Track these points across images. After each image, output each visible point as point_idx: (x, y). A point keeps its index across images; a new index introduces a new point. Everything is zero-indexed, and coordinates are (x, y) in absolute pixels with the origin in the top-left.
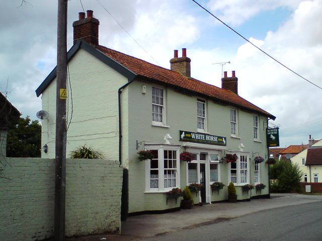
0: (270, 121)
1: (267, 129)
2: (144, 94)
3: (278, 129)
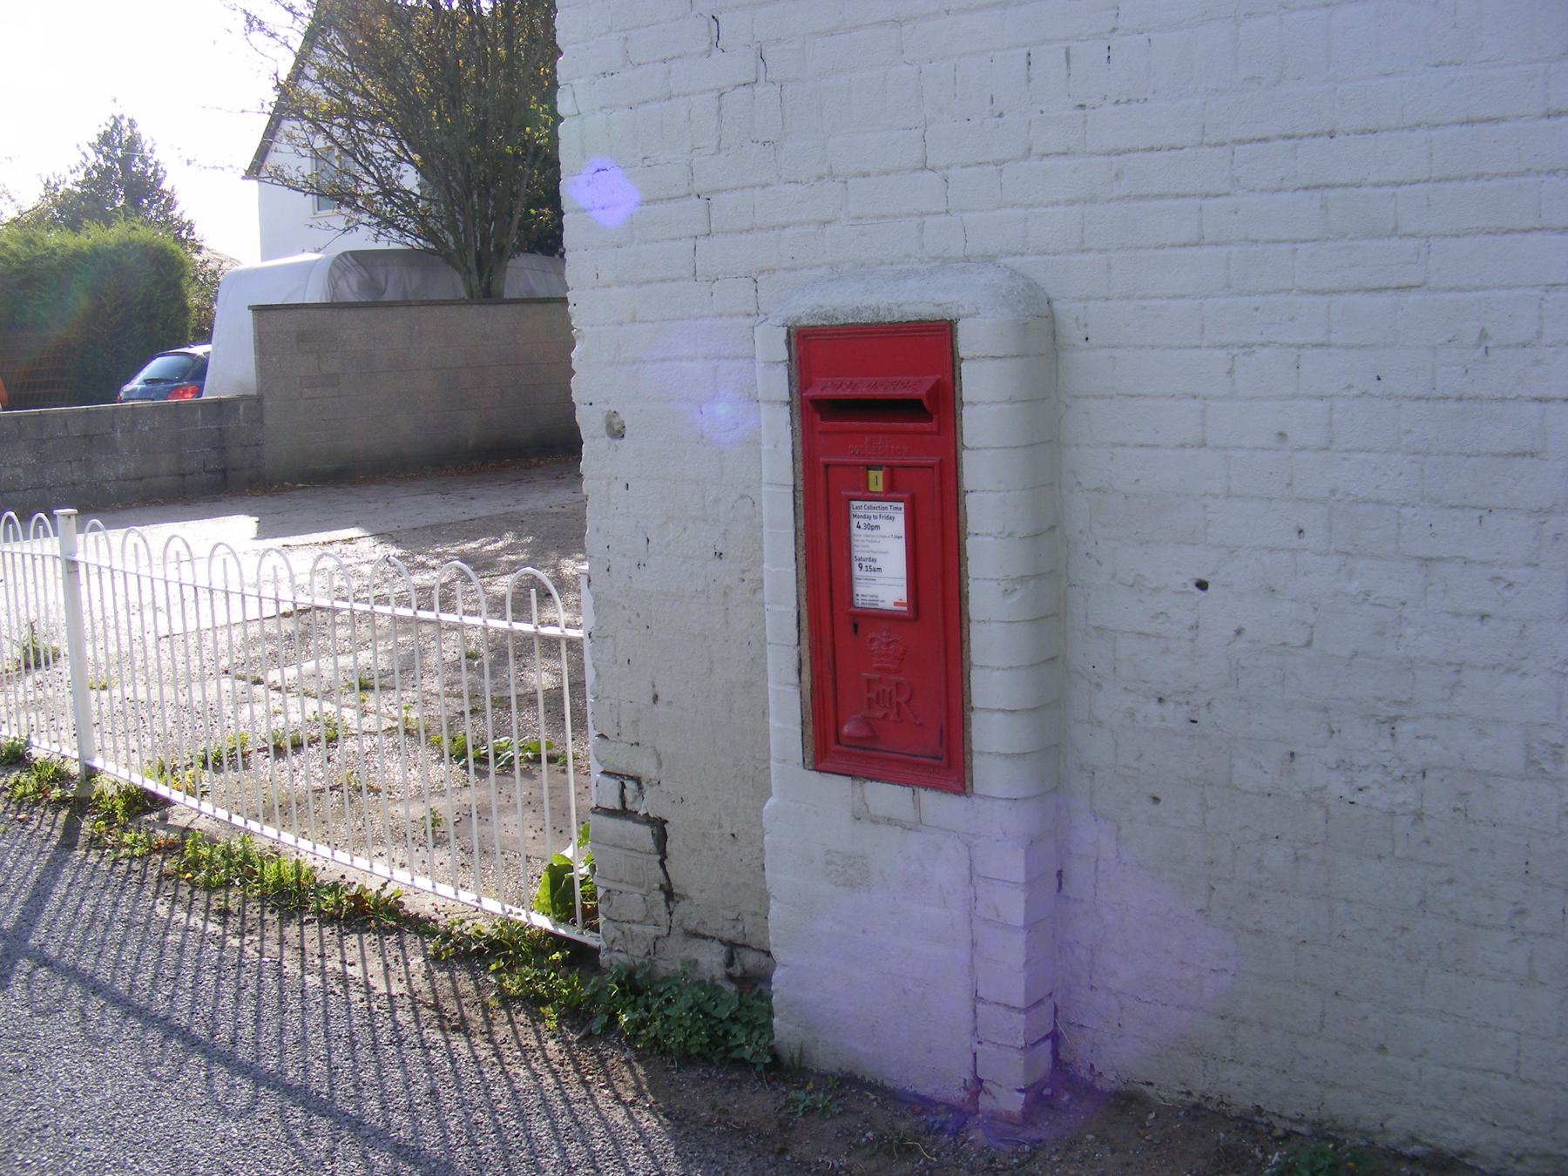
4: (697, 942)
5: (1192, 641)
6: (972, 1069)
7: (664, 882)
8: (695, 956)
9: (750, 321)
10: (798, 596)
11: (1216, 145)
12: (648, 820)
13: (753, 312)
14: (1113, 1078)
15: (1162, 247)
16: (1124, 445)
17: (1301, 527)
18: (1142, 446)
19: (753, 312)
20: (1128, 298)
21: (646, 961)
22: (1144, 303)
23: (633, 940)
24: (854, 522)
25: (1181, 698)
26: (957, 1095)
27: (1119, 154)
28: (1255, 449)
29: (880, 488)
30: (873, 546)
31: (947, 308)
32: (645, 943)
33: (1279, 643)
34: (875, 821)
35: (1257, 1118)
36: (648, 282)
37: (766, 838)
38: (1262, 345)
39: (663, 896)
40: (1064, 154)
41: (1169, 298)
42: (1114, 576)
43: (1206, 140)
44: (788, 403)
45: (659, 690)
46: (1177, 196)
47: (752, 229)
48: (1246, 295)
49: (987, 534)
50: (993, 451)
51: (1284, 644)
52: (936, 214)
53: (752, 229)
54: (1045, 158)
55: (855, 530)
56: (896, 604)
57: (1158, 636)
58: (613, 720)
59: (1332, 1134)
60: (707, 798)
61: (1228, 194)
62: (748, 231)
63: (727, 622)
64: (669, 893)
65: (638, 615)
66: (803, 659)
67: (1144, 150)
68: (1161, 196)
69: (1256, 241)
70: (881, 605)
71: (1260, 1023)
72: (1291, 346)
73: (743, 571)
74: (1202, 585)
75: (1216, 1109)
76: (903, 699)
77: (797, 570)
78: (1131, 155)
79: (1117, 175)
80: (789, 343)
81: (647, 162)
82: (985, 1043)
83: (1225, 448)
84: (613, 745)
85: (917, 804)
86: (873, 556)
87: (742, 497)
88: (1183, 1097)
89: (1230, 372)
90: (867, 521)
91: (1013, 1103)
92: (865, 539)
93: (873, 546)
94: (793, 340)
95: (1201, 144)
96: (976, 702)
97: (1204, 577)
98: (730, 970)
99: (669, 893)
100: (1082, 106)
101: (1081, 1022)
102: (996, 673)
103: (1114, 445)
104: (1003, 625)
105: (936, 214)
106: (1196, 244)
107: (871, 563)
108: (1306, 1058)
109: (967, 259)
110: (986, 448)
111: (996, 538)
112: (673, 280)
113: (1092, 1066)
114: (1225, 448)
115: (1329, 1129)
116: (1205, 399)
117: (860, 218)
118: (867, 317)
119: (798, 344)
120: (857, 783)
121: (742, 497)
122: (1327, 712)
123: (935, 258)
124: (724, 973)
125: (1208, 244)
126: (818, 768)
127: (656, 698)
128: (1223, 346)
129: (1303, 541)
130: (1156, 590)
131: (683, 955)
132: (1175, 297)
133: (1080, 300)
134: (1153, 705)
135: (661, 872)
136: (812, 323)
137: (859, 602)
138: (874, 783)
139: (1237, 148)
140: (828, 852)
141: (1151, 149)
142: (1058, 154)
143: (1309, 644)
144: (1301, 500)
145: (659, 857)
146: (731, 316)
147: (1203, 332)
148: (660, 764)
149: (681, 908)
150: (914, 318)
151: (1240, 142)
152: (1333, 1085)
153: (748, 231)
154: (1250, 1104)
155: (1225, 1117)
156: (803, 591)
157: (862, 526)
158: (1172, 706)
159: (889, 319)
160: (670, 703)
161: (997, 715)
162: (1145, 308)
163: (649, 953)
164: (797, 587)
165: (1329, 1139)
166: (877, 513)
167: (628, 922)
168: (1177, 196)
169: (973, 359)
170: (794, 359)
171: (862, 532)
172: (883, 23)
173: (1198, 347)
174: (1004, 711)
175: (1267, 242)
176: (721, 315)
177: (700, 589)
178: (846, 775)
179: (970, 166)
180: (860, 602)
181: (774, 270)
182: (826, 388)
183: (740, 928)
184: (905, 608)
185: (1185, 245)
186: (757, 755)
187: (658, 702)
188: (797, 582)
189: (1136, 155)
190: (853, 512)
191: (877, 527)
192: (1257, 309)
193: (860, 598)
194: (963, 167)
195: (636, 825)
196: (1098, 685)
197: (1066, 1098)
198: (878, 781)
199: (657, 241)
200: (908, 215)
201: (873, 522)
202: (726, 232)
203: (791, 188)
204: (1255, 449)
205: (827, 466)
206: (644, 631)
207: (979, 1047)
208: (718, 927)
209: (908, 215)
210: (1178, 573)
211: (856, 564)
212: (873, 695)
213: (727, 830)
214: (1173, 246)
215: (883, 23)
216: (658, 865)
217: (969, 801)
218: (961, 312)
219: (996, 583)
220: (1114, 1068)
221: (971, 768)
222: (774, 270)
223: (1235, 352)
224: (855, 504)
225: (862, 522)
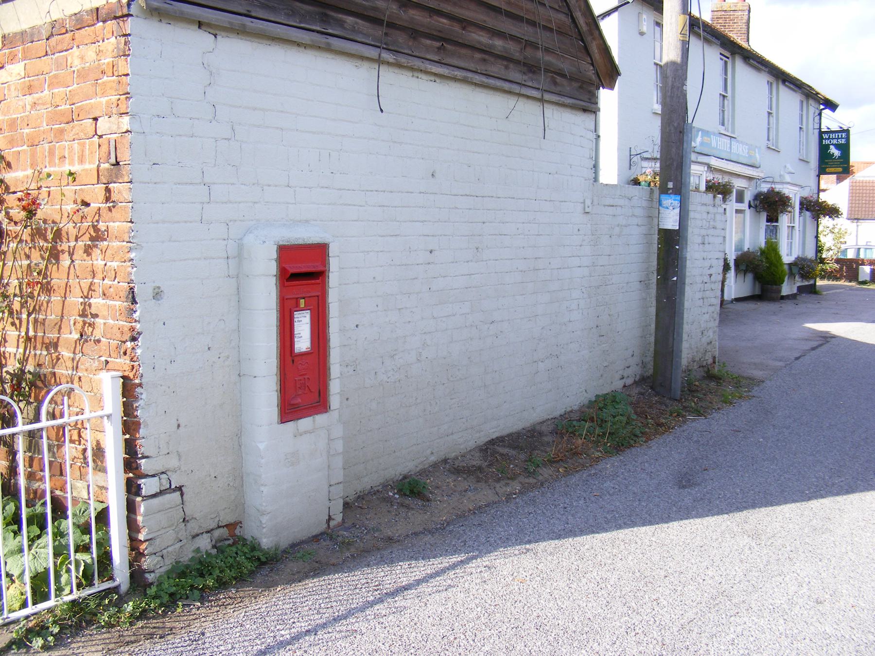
0: (827, 112)
1: (821, 133)
2: (642, 34)
3: (847, 132)
8: (198, 546)
9: (225, 242)
13: (226, 238)
19: (226, 238)
36: (178, 222)
44: (275, 275)
45: (180, 422)
56: (306, 349)
58: (156, 446)
62: (226, 203)
70: (302, 350)
73: (220, 354)
81: (181, 165)
84: (155, 459)
86: (300, 332)
87: (220, 320)
100: (332, 173)
118: (301, 242)
121: (220, 320)
123: (292, 220)
127: (179, 426)
139: (367, 193)
151: (367, 191)
153: (226, 203)
172: (277, 128)
176: (213, 239)
181: (236, 221)
182: (293, 269)
187: (180, 428)
190: (295, 316)
201: (300, 319)
203: (243, 186)
206: (173, 394)
215: (277, 128)
221: (329, 402)
222: (236, 221)
224: (295, 313)
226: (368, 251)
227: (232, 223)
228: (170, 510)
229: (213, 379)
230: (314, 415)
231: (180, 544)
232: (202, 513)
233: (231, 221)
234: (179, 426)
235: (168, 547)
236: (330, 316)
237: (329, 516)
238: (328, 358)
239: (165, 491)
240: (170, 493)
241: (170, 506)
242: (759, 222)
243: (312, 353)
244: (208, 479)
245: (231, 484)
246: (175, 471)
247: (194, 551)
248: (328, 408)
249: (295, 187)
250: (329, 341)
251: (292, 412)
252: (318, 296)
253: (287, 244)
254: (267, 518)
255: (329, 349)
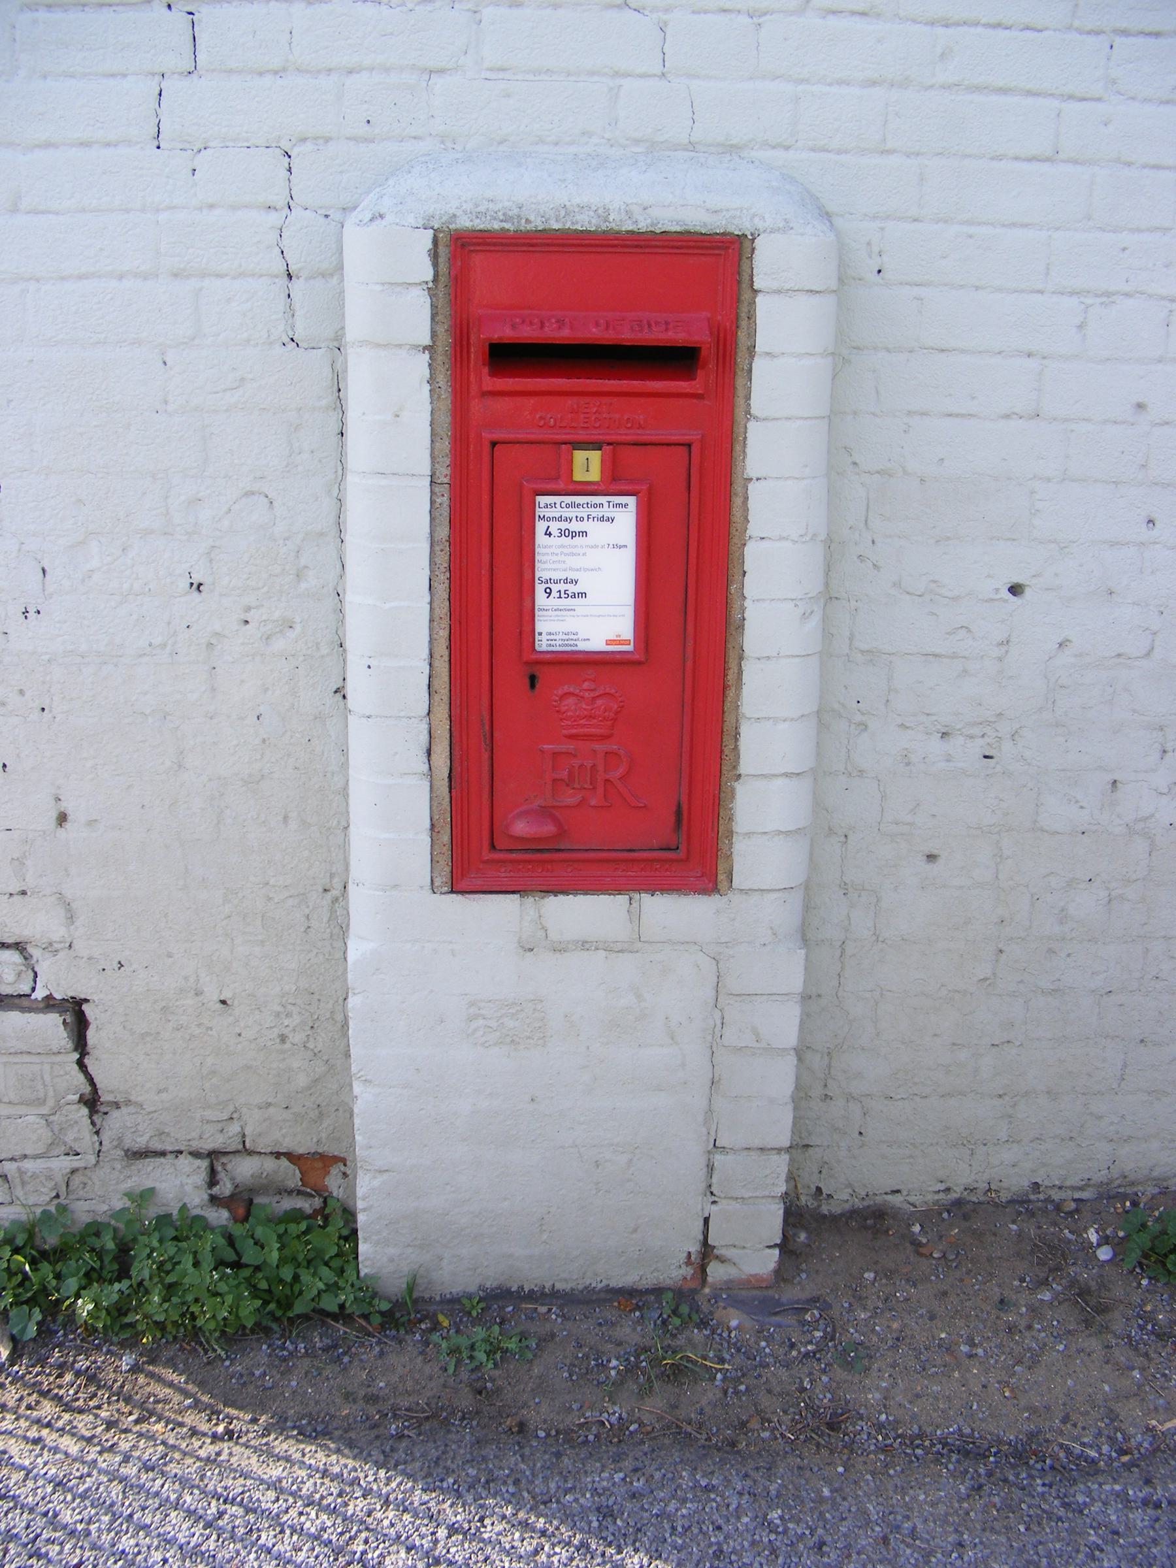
4: (150, 1163)
5: (1000, 659)
6: (701, 1237)
7: (87, 1089)
8: (149, 1184)
9: (274, 218)
10: (431, 641)
11: (1089, 33)
12: (50, 1004)
14: (845, 1197)
15: (998, 158)
16: (924, 414)
17: (1154, 516)
18: (950, 415)
20: (946, 222)
21: (52, 1209)
22: (972, 230)
23: (23, 1183)
24: (540, 527)
25: (977, 731)
26: (674, 1272)
27: (947, 26)
28: (1105, 422)
29: (594, 475)
30: (572, 562)
31: (734, 217)
32: (51, 1184)
33: (1113, 654)
34: (559, 949)
35: (1032, 1197)
37: (352, 1001)
38: (1127, 295)
39: (85, 1111)
40: (863, 14)
41: (1004, 226)
42: (897, 585)
43: (1076, 23)
44: (425, 348)
45: (68, 806)
46: (1030, 93)
47: (284, 69)
48: (1110, 231)
49: (782, 538)
50: (799, 423)
51: (1119, 655)
52: (642, 76)
53: (284, 69)
54: (830, 17)
55: (540, 538)
56: (609, 642)
57: (954, 656)
59: (1121, 1190)
60: (170, 955)
61: (1099, 100)
62: (276, 73)
63: (213, 689)
64: (92, 1102)
65: (21, 692)
66: (436, 734)
67: (988, 26)
68: (1003, 91)
69: (1129, 164)
70: (582, 646)
71: (1048, 1093)
72: (1163, 298)
73: (248, 609)
74: (1015, 590)
75: (982, 1199)
76: (615, 775)
77: (431, 603)
78: (965, 28)
79: (943, 54)
80: (434, 255)
82: (724, 1202)
83: (1066, 420)
85: (635, 917)
86: (572, 575)
87: (249, 494)
88: (941, 1196)
89: (1080, 327)
90: (564, 525)
91: (765, 1262)
92: (558, 551)
93: (572, 562)
94: (444, 252)
95: (1069, 28)
96: (746, 765)
97: (1016, 579)
98: (216, 1190)
99: (92, 1102)
101: (806, 1142)
102: (782, 726)
103: (910, 413)
104: (797, 660)
105: (642, 76)
106: (1047, 160)
107: (567, 586)
108: (1100, 1118)
109: (692, 146)
110: (788, 419)
111: (795, 542)
112: (108, 145)
113: (819, 1189)
114: (1066, 420)
115: (1119, 1186)
116: (1044, 358)
117: (503, 70)
118: (585, 222)
119: (453, 258)
120: (530, 900)
121: (249, 494)
122: (1162, 730)
123: (637, 142)
124: (206, 1197)
125: (1063, 161)
126: (455, 888)
127: (62, 818)
128: (1072, 293)
129: (1156, 532)
130: (955, 599)
131: (128, 1185)
132: (1013, 225)
133: (875, 218)
134: (936, 746)
135: (81, 1077)
136: (480, 224)
137: (543, 644)
138: (561, 897)
139: (1118, 41)
140: (472, 1004)
141: (998, 25)
142: (853, 13)
143: (1148, 654)
144: (1156, 484)
145: (77, 1056)
146: (234, 208)
147: (1047, 274)
148: (71, 918)
149: (115, 1123)
150: (678, 229)
152: (1128, 1139)
153: (276, 73)
154: (1026, 1184)
155: (996, 1205)
156: (443, 634)
157: (555, 532)
158: (960, 740)
159: (628, 226)
160: (91, 823)
161: (780, 782)
162: (971, 237)
163: (57, 1196)
164: (431, 629)
165: (1123, 1197)
166: (582, 512)
167: (12, 1159)
168: (1030, 93)
169: (778, 292)
170: (443, 280)
171: (554, 541)
173: (1041, 292)
174: (786, 775)
175: (1144, 166)
177: (158, 640)
178: (513, 892)
179: (706, 12)
180: (544, 643)
181: (327, 140)
183: (235, 1128)
184: (630, 648)
185: (1030, 160)
186: (272, 882)
187: (68, 825)
188: (431, 621)
189: (972, 30)
190: (539, 512)
191: (584, 533)
192: (1124, 249)
193: (544, 637)
194: (694, 12)
195: (27, 1015)
196: (863, 726)
197: (803, 1236)
198: (565, 892)
199: (72, 76)
200: (592, 73)
201: (575, 526)
202: (231, 71)
204: (1105, 422)
205: (494, 444)
207: (714, 1207)
208: (194, 1135)
209: (592, 73)
210: (989, 576)
211: (540, 589)
212: (564, 774)
213: (212, 995)
214: (1017, 158)
216: (76, 1067)
217: (725, 899)
218: (760, 225)
219: (792, 604)
220: (849, 1185)
221: (729, 857)
222: (327, 140)
223: (1089, 301)
224: (542, 500)
225: (554, 527)
226: (1108, 294)
227: (309, 146)
228: (27, 1058)
229: (213, 689)
230: (639, 891)
231: (68, 1163)
232: (164, 1095)
233: (304, 140)
234: (62, 818)
235: (25, 1156)
236: (753, 529)
237: (705, 1242)
238: (731, 693)
239: (17, 1001)
240: (23, 1010)
241: (25, 1049)
242: (799, 1147)
243: (639, 663)
244: (190, 1001)
245: (298, 1038)
246: (50, 948)
247: (128, 1195)
248: (721, 877)
249: (667, 10)
250: (741, 627)
251: (529, 861)
252: (689, 446)
253: (496, 226)
254: (376, 1183)
255: (741, 658)
